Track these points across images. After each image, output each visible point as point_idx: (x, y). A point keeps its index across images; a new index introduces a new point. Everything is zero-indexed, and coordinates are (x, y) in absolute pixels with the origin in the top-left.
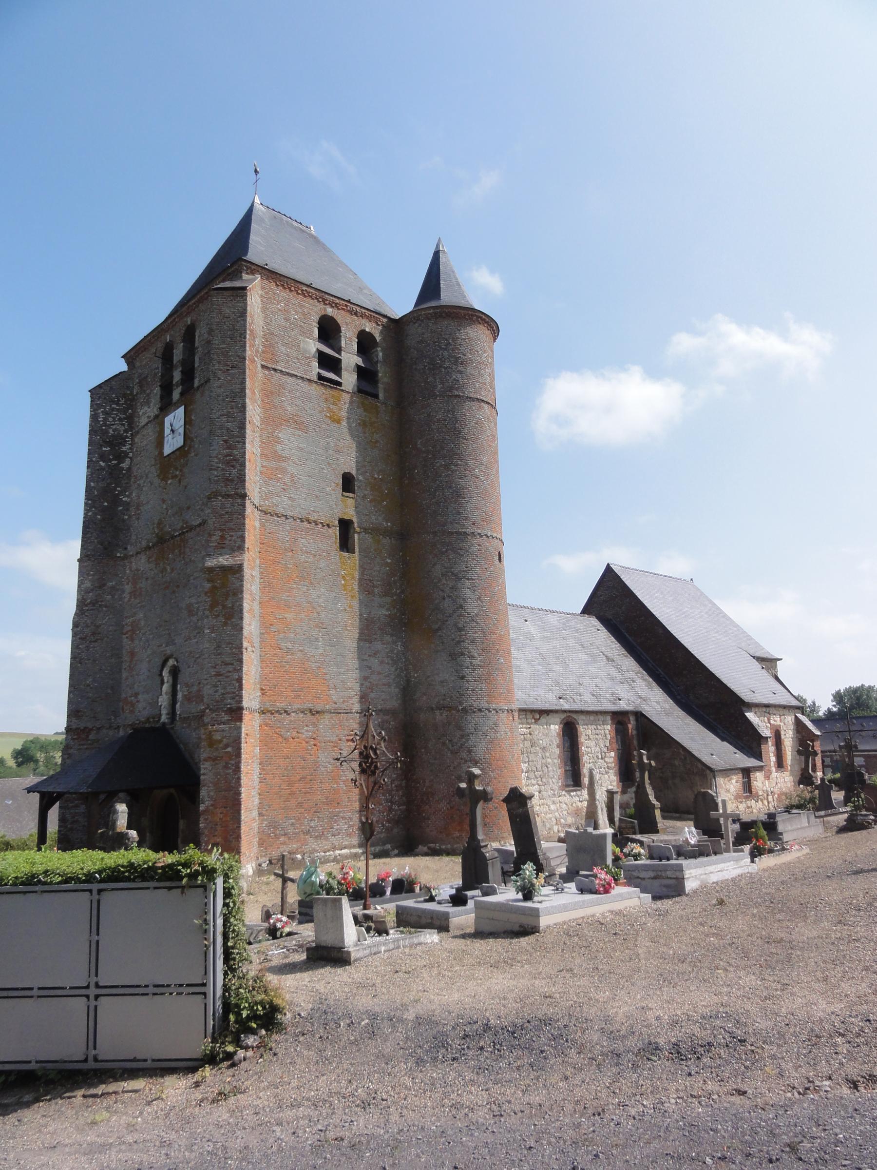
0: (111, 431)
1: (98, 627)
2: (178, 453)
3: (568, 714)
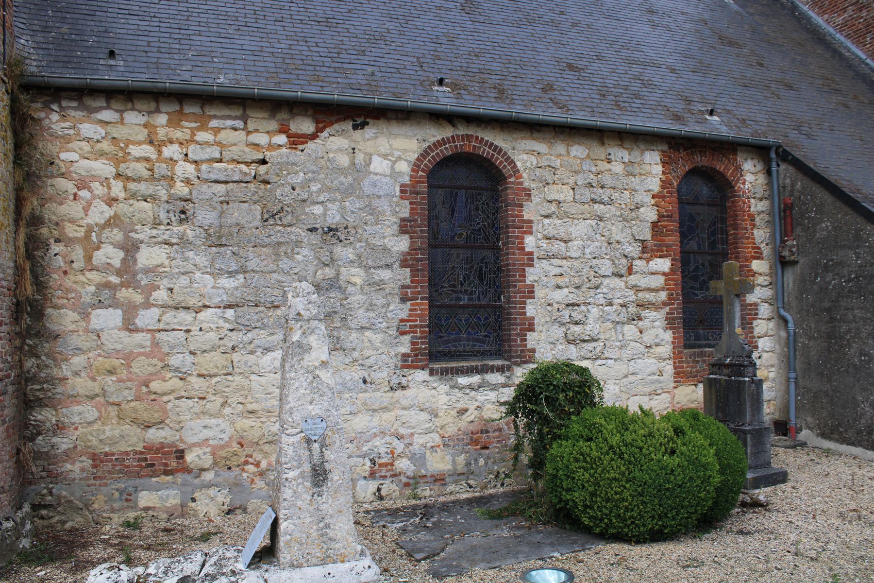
3: (701, 160)
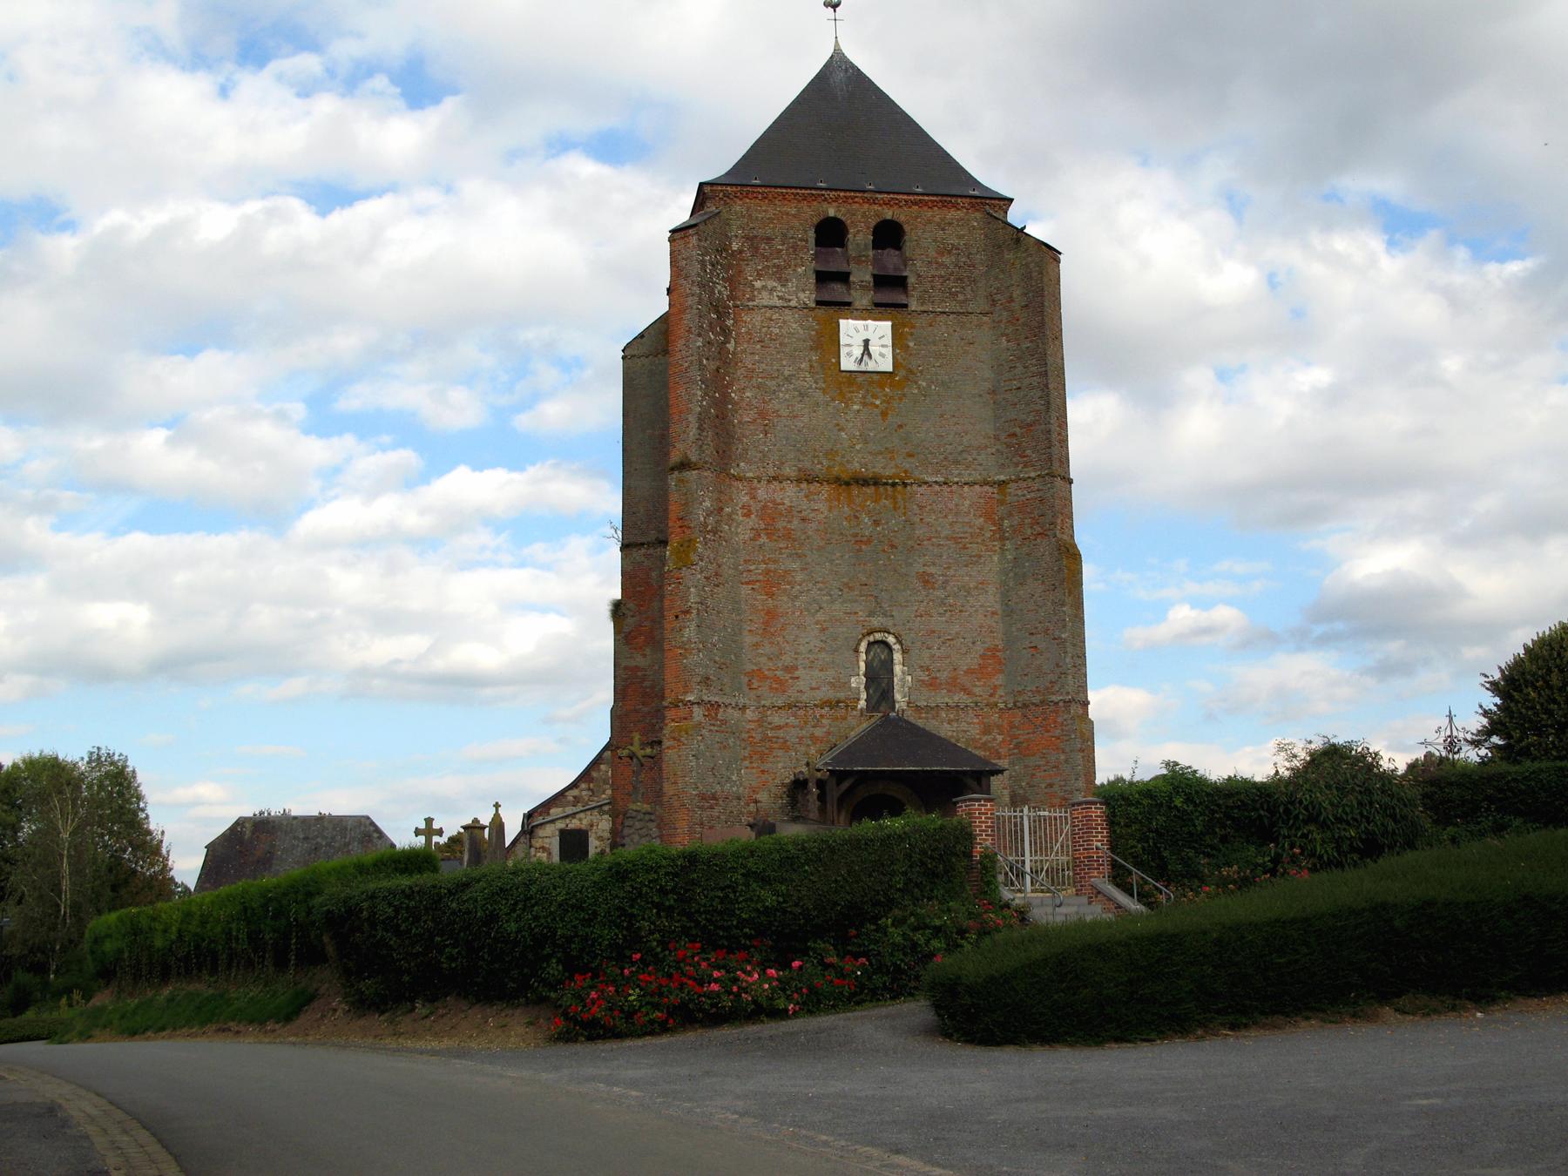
2: (876, 377)
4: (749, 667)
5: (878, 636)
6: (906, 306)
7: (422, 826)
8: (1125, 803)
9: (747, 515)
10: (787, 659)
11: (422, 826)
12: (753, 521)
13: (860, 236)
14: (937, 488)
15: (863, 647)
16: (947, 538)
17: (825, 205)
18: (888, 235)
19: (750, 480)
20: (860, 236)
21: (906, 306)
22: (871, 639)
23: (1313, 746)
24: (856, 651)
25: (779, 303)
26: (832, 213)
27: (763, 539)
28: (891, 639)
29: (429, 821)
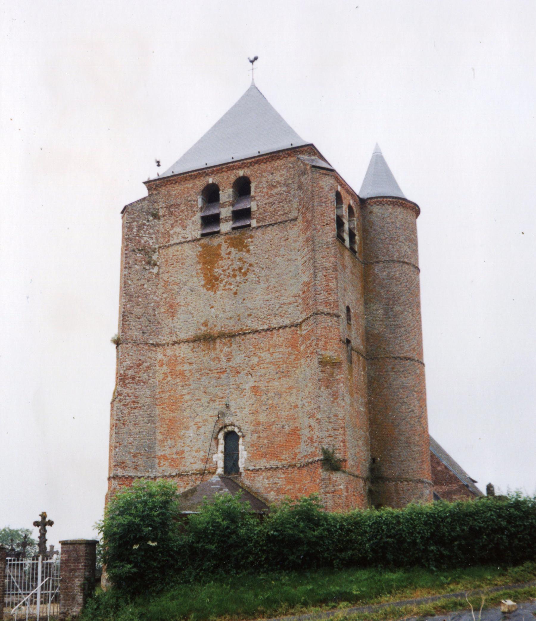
0: (142, 241)
1: (137, 397)
4: (159, 453)
5: (230, 428)
6: (249, 226)
7: (39, 519)
8: (225, 473)
9: (161, 366)
10: (179, 447)
11: (39, 519)
12: (165, 369)
13: (226, 194)
14: (263, 333)
15: (221, 436)
16: (271, 363)
17: (207, 177)
18: (242, 188)
19: (163, 345)
20: (226, 194)
21: (249, 226)
22: (226, 430)
23: (519, 499)
24: (216, 439)
25: (183, 240)
26: (210, 181)
27: (169, 378)
28: (236, 430)
29: (44, 516)
